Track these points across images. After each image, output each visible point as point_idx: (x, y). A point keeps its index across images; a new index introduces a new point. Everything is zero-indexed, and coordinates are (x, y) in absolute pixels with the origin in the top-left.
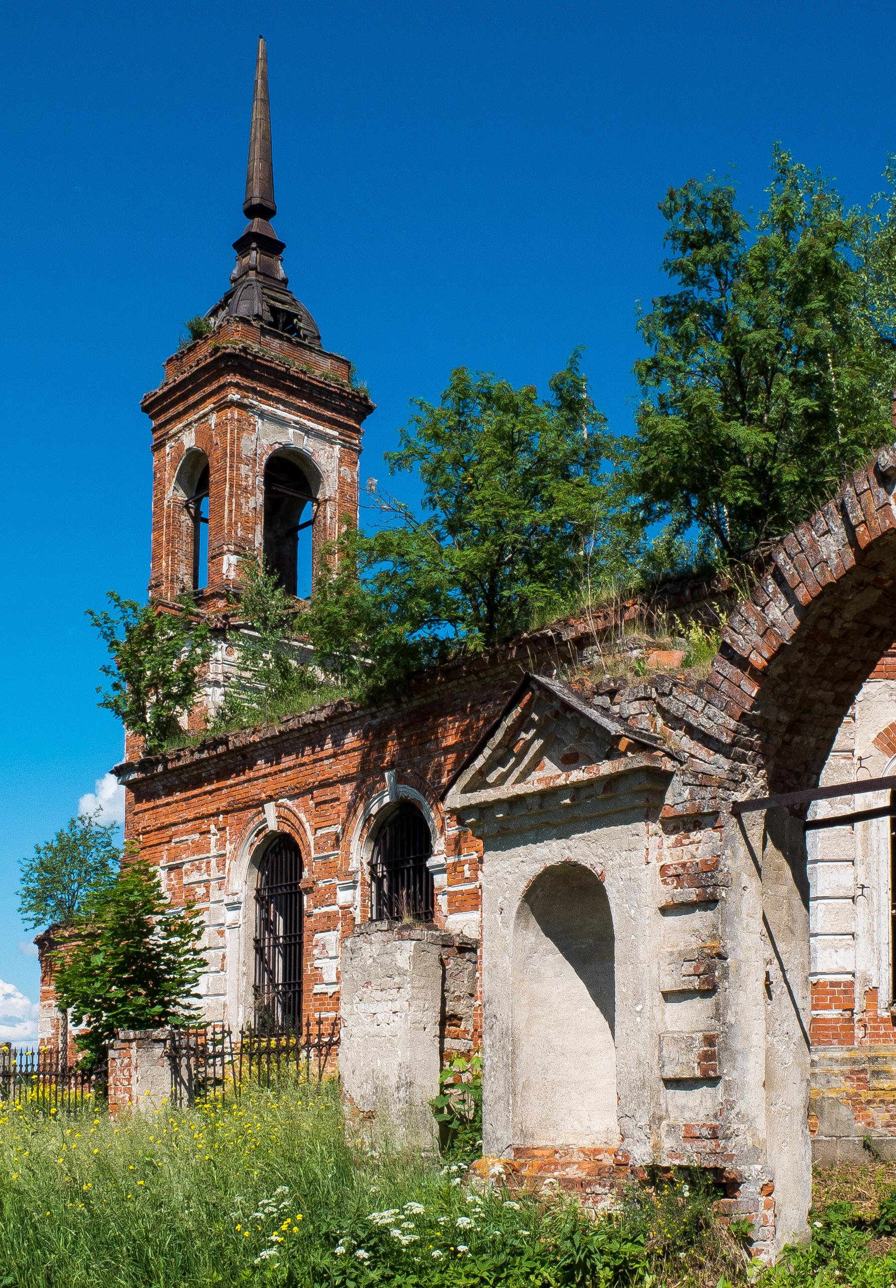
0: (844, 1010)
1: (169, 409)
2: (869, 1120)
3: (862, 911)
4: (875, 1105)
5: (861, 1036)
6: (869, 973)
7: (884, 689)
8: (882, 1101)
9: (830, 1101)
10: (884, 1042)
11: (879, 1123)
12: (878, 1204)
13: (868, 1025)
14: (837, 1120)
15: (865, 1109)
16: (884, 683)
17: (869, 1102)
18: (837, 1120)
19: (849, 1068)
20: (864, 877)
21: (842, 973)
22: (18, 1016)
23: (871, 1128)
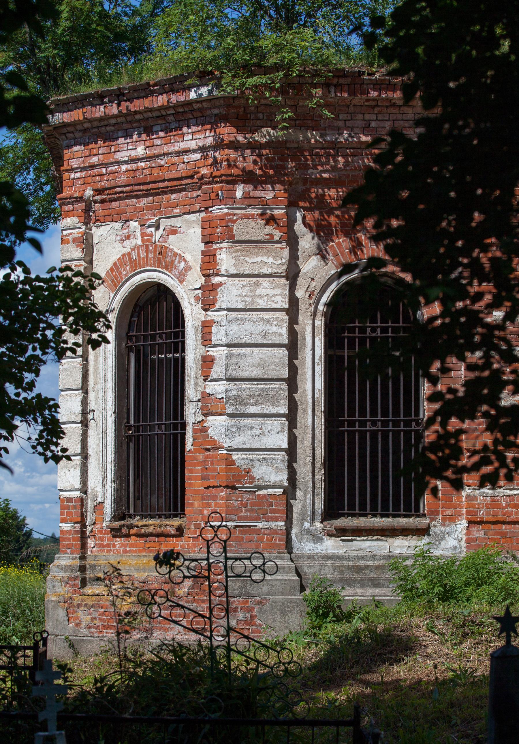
0: (75, 523)
1: (43, 278)
2: (78, 621)
3: (93, 434)
4: (82, 608)
5: (92, 546)
6: (96, 489)
7: (112, 230)
8: (86, 605)
9: (53, 604)
10: (108, 551)
11: (83, 625)
12: (440, 608)
13: (97, 536)
14: (57, 621)
15: (77, 612)
16: (111, 226)
17: (79, 605)
18: (57, 621)
19: (67, 574)
20: (94, 404)
21: (70, 490)
22: (295, 550)
23: (78, 629)
